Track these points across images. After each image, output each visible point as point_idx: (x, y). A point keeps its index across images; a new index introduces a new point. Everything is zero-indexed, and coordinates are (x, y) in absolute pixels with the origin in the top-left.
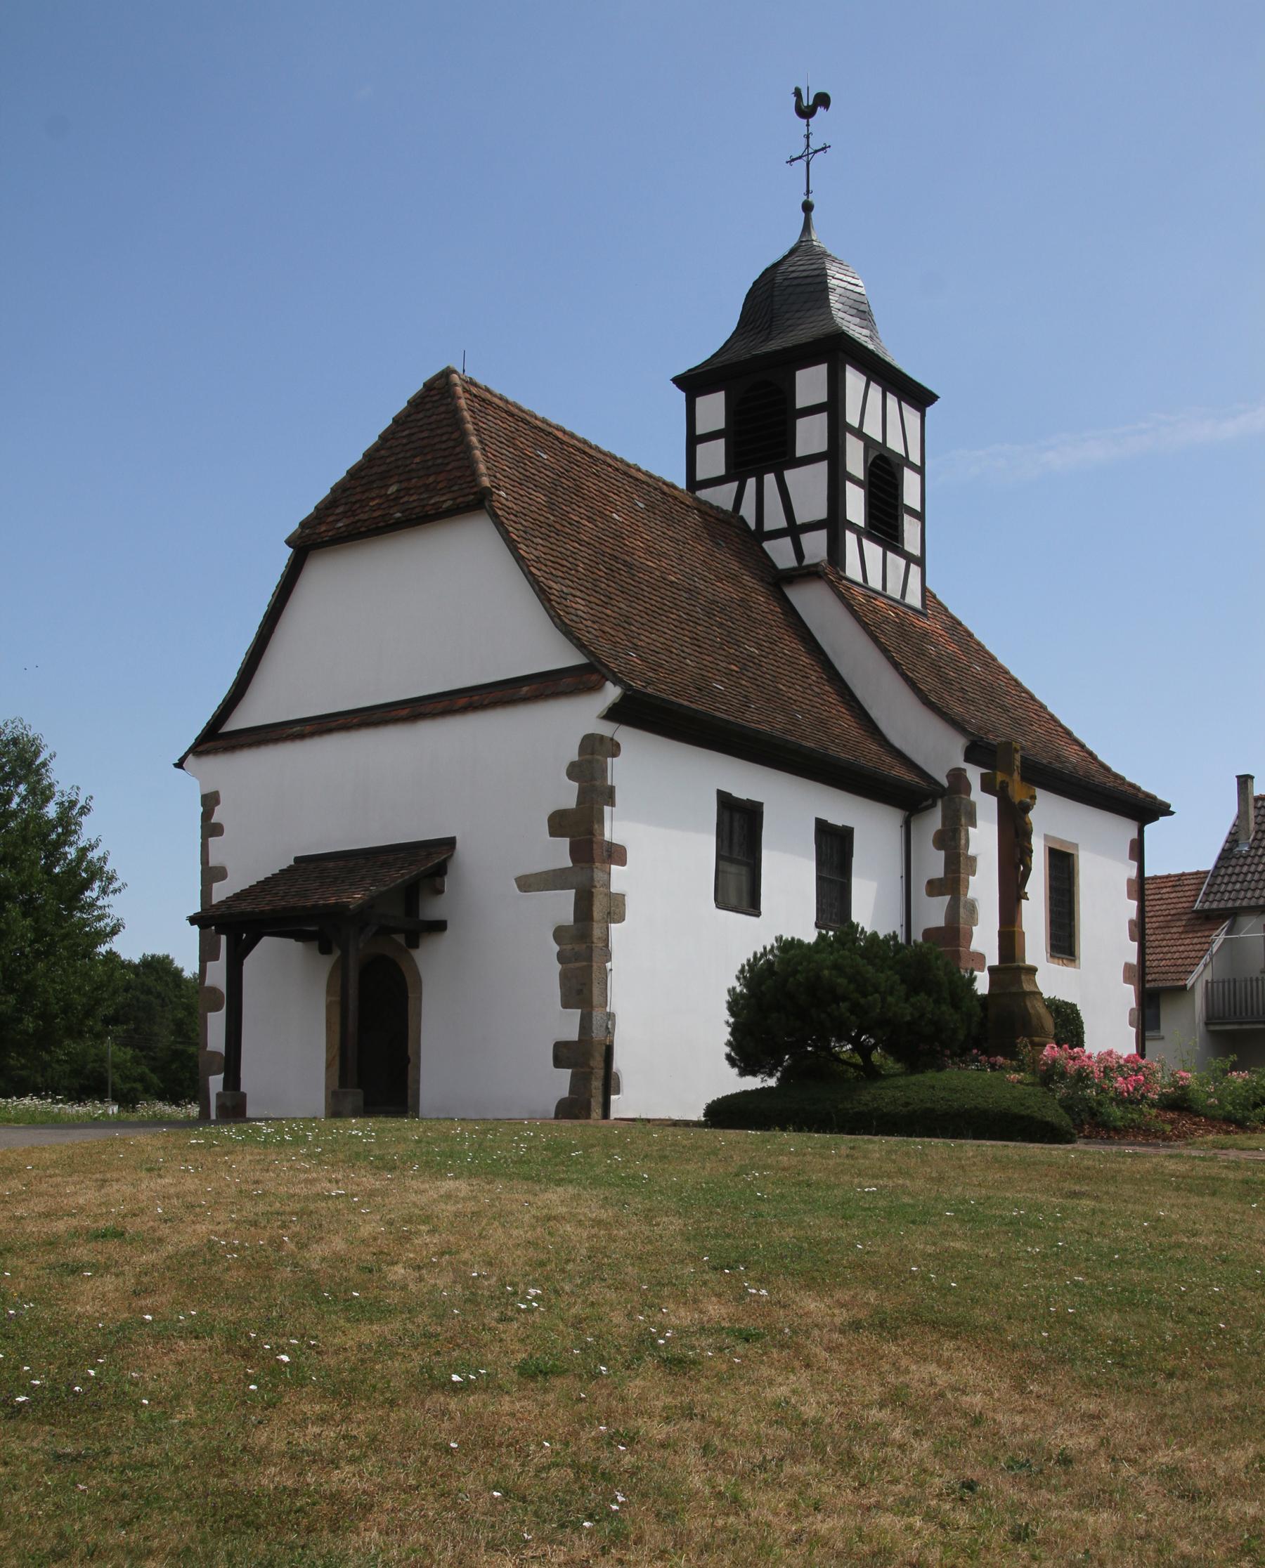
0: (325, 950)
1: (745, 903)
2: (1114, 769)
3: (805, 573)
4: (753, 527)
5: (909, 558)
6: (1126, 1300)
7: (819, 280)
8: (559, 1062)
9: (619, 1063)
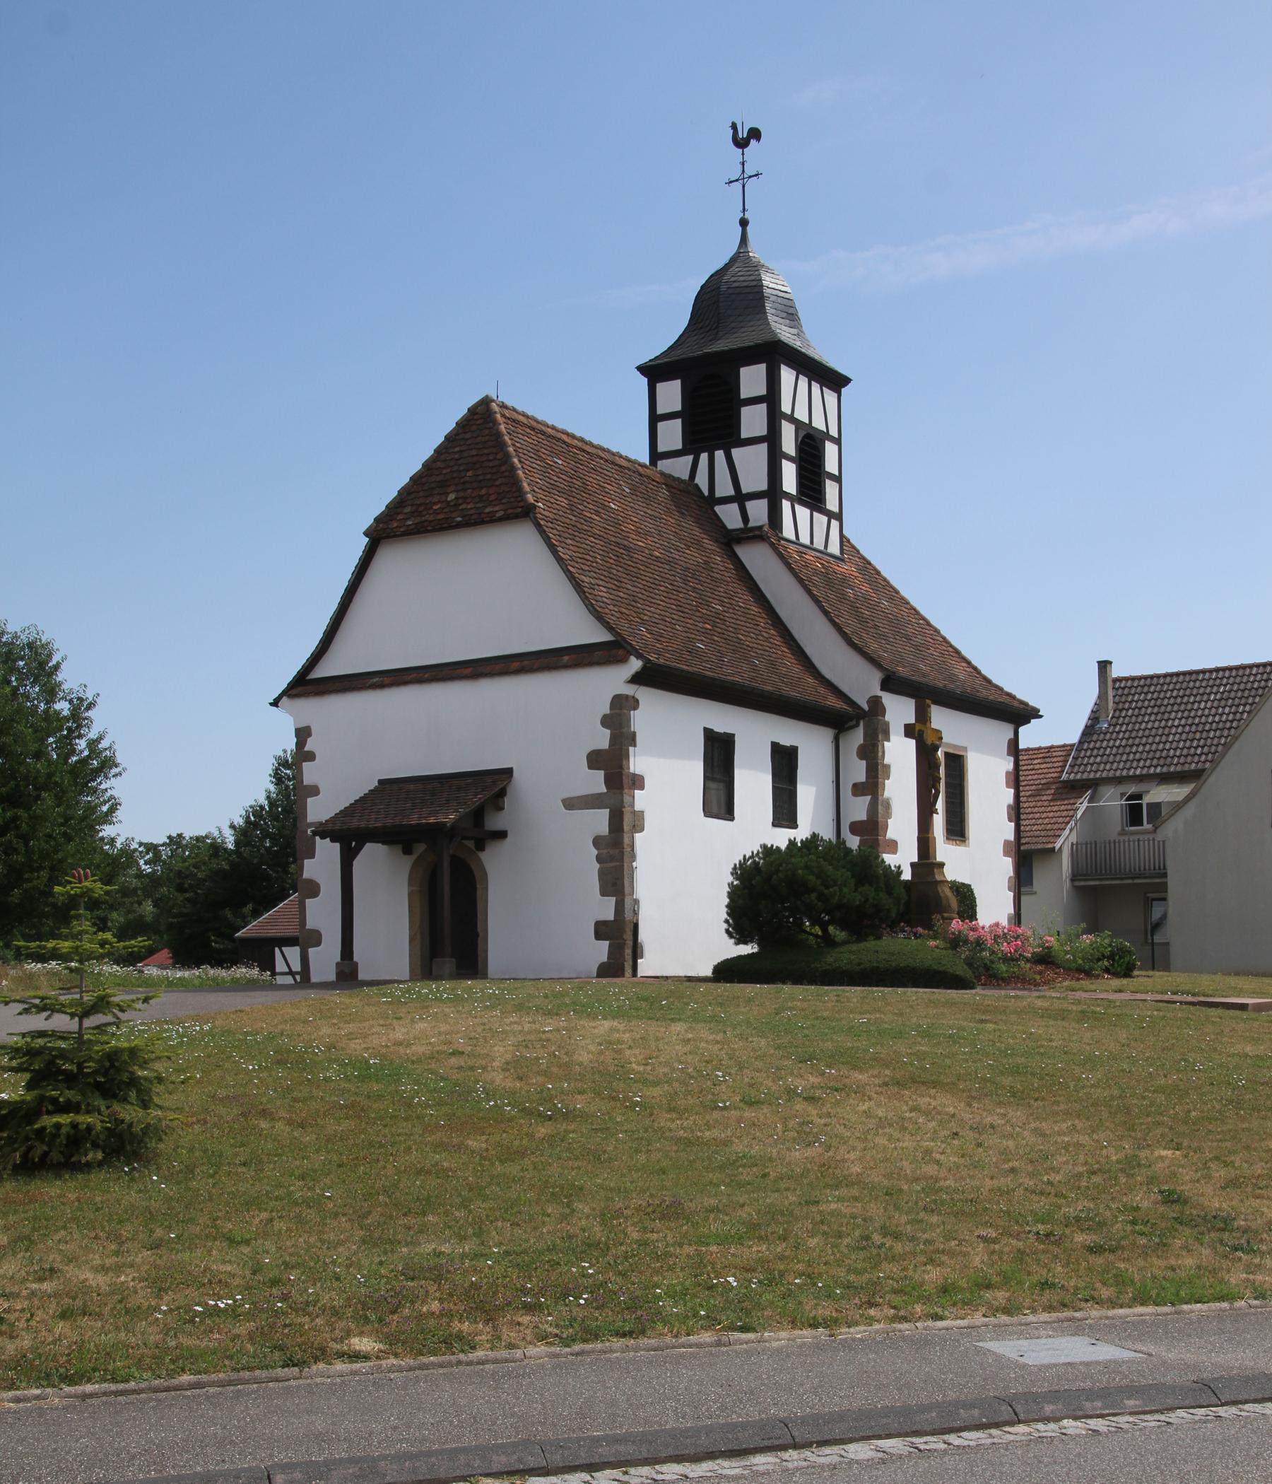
0: (407, 851)
1: (723, 811)
2: (995, 681)
3: (750, 535)
4: (706, 493)
5: (830, 515)
6: (1016, 1071)
7: (756, 290)
8: (599, 936)
9: (642, 936)
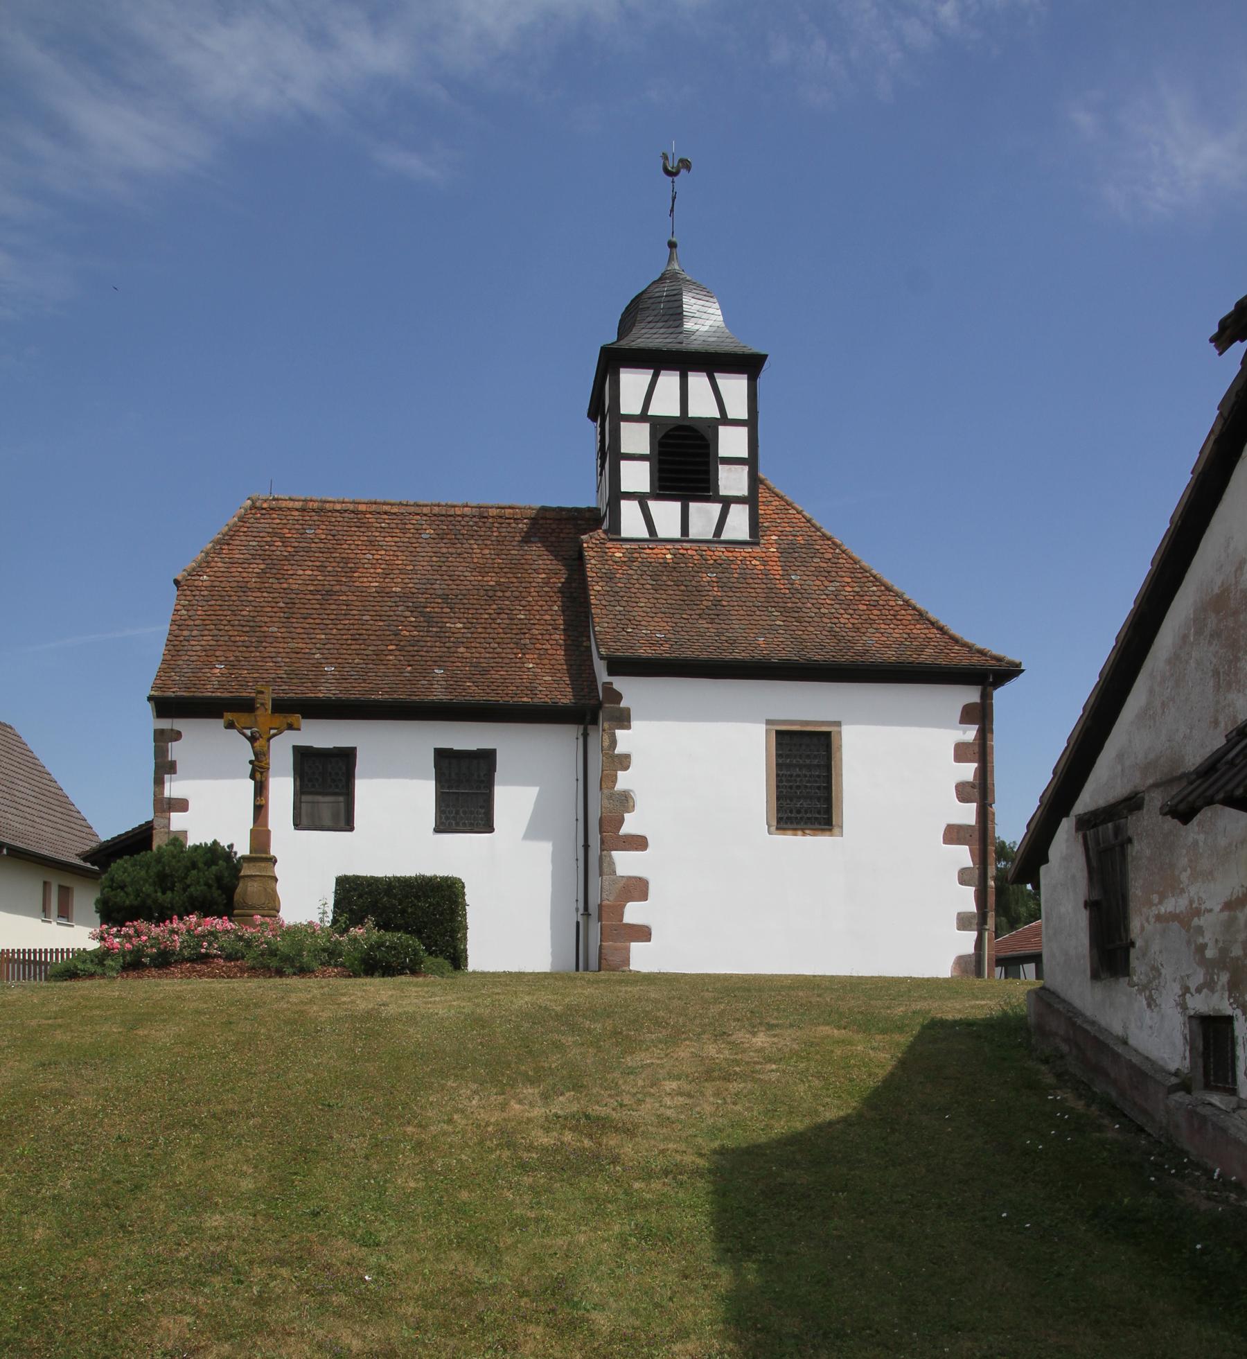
1: (342, 823)
